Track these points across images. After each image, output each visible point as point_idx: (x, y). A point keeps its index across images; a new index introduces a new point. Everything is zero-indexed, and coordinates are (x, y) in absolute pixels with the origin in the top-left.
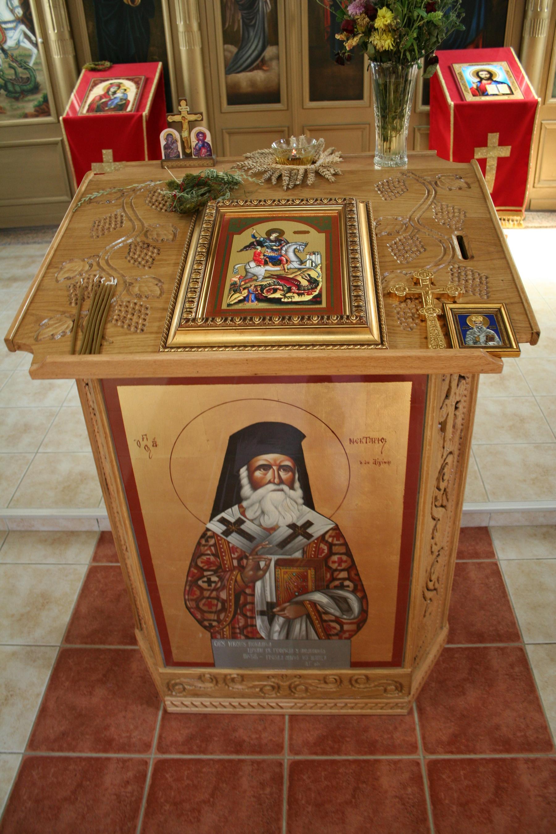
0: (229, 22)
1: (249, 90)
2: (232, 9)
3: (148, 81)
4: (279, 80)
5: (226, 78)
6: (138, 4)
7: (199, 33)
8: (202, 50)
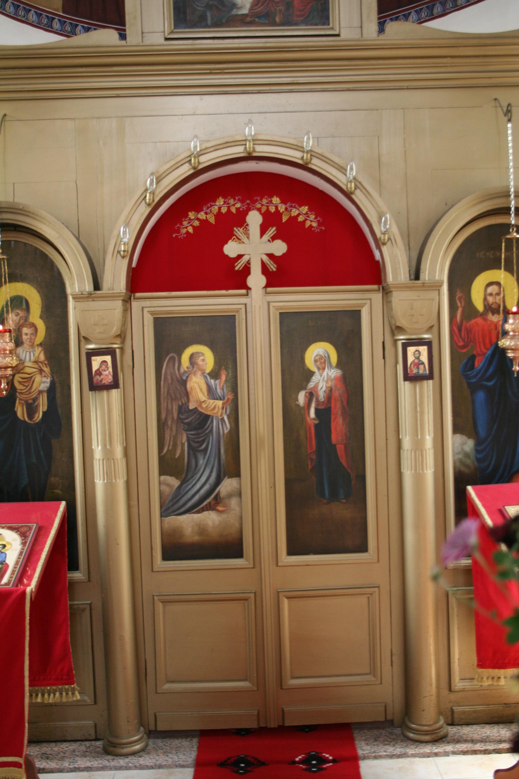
0: (169, 446)
1: (196, 538)
2: (174, 428)
3: (41, 532)
4: (241, 524)
5: (161, 522)
6: (37, 421)
7: (124, 460)
8: (128, 483)
